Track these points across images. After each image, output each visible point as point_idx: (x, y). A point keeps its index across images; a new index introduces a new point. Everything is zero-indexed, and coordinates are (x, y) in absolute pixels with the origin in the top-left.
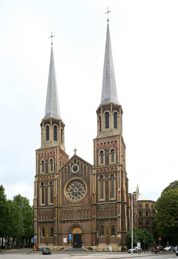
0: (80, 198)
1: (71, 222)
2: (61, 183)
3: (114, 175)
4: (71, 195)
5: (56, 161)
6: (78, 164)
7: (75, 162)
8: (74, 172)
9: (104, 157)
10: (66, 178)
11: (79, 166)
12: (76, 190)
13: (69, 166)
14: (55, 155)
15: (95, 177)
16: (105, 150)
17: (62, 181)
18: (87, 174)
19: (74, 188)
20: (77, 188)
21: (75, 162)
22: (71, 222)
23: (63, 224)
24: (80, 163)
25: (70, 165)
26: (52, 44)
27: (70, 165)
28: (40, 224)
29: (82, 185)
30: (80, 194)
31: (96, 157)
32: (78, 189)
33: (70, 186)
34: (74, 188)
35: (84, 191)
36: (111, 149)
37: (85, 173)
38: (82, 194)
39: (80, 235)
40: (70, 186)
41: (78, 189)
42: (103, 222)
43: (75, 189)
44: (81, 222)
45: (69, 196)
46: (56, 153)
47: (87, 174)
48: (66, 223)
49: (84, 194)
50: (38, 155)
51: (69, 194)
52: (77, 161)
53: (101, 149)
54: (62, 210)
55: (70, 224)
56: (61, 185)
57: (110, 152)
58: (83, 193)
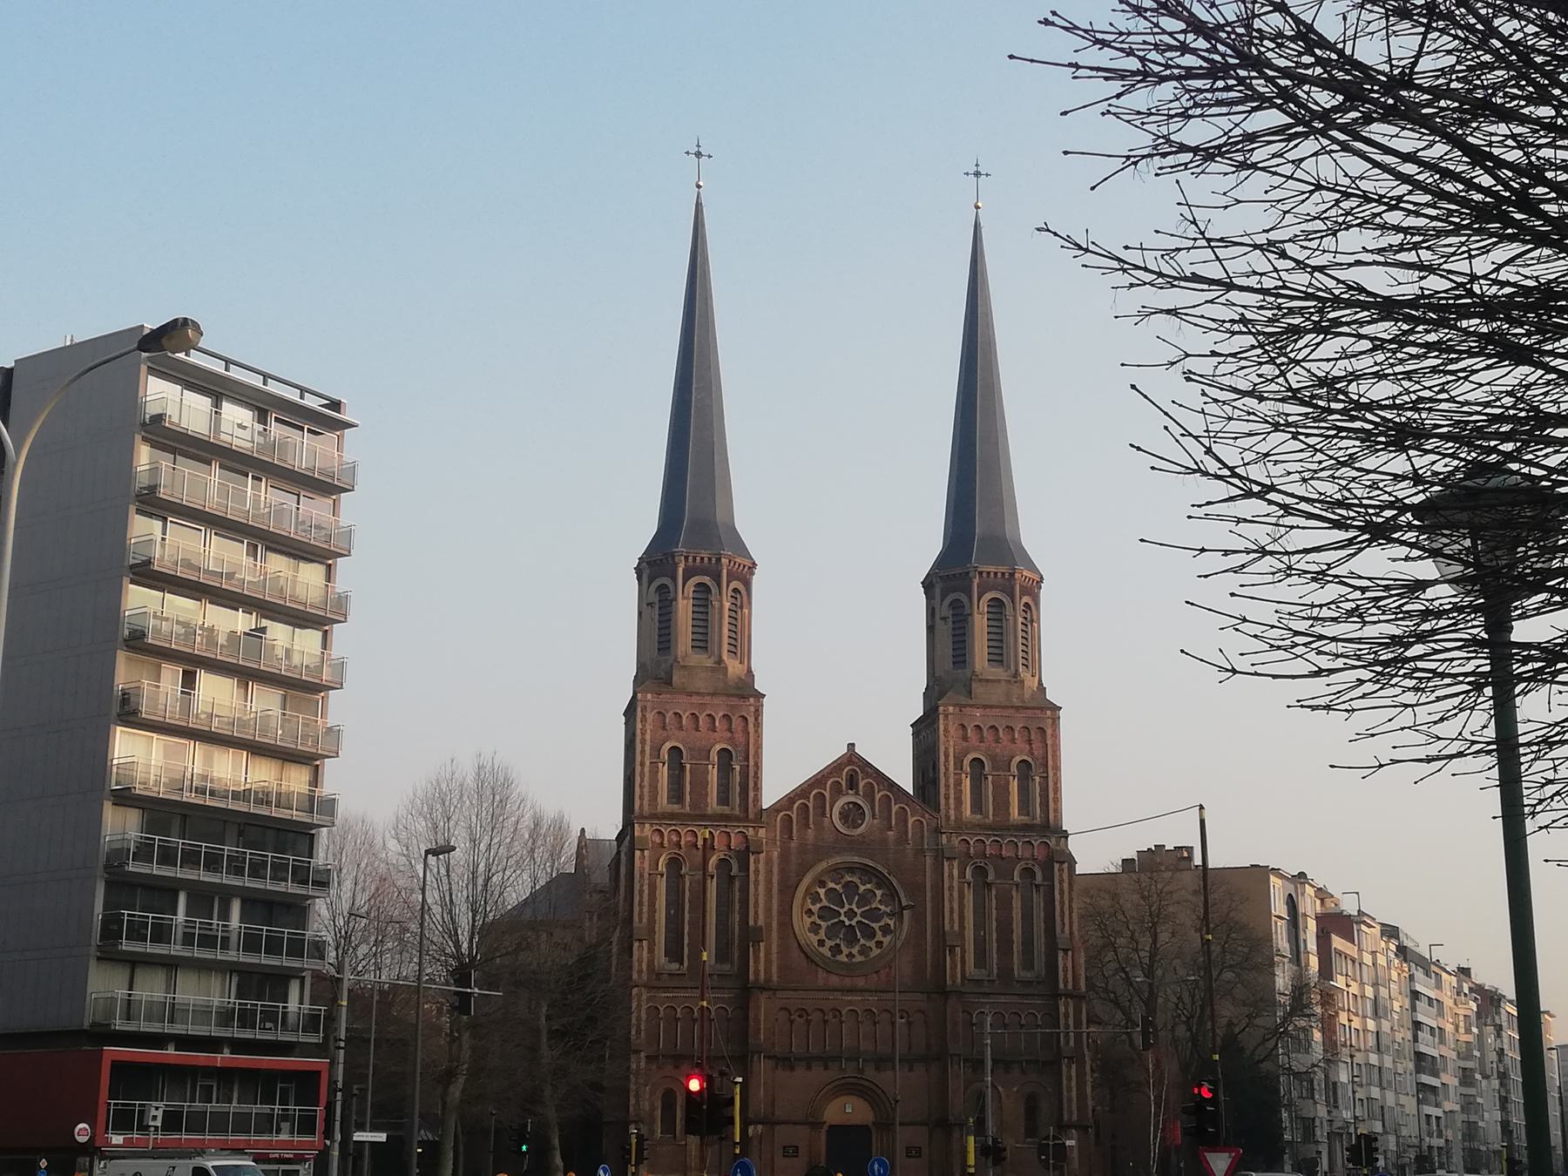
0: (811, 935)
1: (826, 1068)
3: (1033, 874)
4: (822, 932)
7: (852, 783)
8: (838, 825)
11: (873, 809)
12: (851, 914)
16: (993, 758)
19: (863, 915)
20: (858, 918)
21: (852, 783)
22: (826, 1068)
27: (827, 795)
28: (654, 1067)
29: (879, 893)
30: (871, 934)
31: (952, 781)
34: (863, 915)
35: (892, 923)
38: (879, 933)
39: (863, 1130)
40: (822, 891)
41: (859, 911)
43: (847, 907)
45: (814, 939)
49: (889, 938)
51: (815, 928)
53: (976, 749)
57: (1014, 769)
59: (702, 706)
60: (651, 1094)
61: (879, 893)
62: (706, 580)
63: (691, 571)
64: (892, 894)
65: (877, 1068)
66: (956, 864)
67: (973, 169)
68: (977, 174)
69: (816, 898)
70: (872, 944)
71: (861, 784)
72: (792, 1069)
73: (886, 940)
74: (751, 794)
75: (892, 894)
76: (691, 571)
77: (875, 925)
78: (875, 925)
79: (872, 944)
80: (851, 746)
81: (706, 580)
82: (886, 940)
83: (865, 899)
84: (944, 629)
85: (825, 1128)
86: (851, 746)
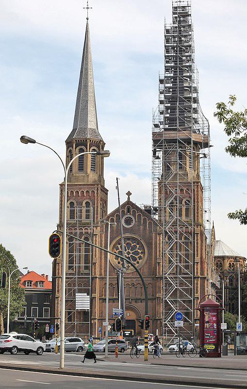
5: (96, 206)
6: (134, 215)
7: (129, 211)
15: (161, 239)
19: (133, 253)
20: (131, 254)
21: (129, 211)
22: (114, 302)
24: (137, 215)
26: (87, 19)
29: (138, 246)
32: (131, 252)
33: (140, 251)
35: (142, 256)
41: (131, 252)
44: (136, 302)
58: (140, 258)
61: (138, 246)
63: (85, 148)
64: (142, 247)
67: (86, 7)
68: (88, 8)
69: (117, 249)
70: (136, 263)
71: (131, 211)
73: (140, 261)
75: (142, 247)
76: (85, 148)
77: (137, 257)
78: (137, 257)
79: (136, 263)
82: (140, 261)
83: (133, 248)
84: (31, 140)
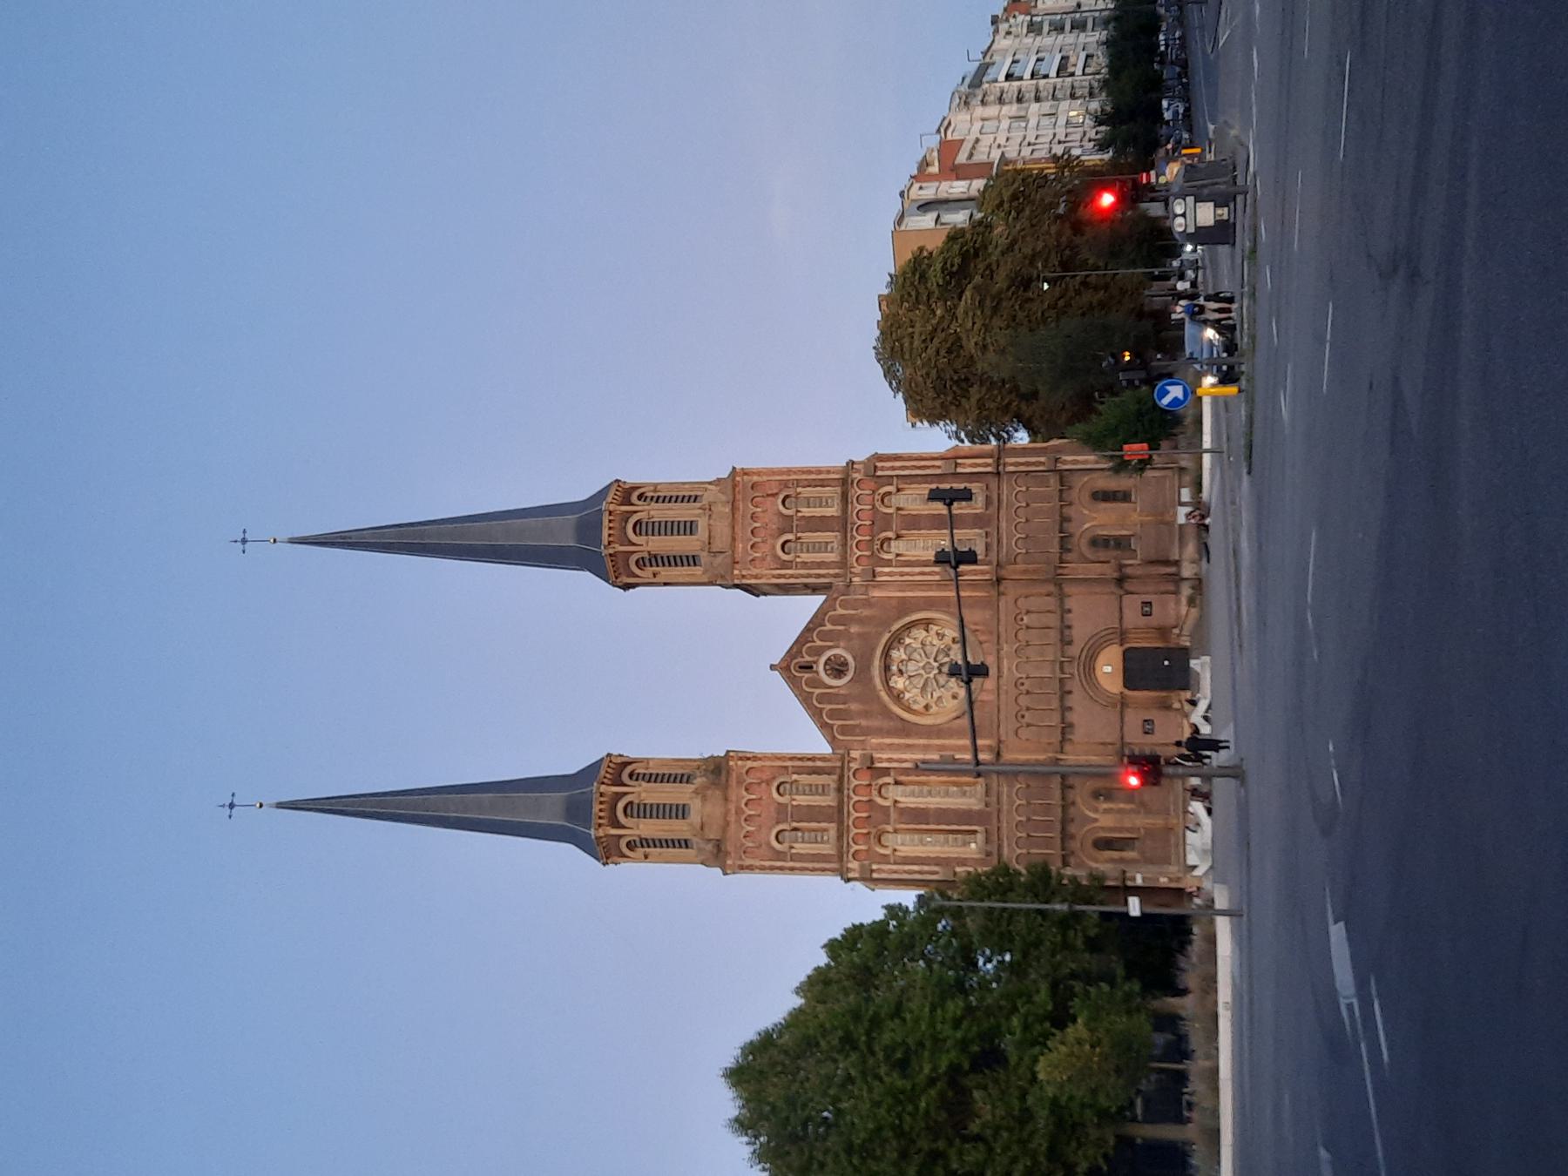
2: (888, 741)
5: (789, 763)
6: (819, 652)
7: (807, 667)
9: (808, 537)
10: (866, 714)
11: (830, 648)
13: (821, 698)
14: (761, 769)
15: (887, 570)
16: (782, 532)
17: (880, 732)
18: (866, 612)
21: (807, 667)
23: (1078, 735)
24: (819, 643)
25: (818, 691)
36: (781, 507)
37: (860, 621)
42: (1075, 539)
46: (755, 764)
47: (866, 612)
48: (1072, 717)
50: (748, 862)
52: (808, 658)
54: (1011, 733)
55: (1076, 699)
56: (896, 741)
59: (739, 811)
60: (1096, 861)
62: (621, 805)
65: (1070, 643)
66: (879, 569)
68: (232, 806)
72: (1071, 725)
74: (819, 764)
80: (772, 667)
81: (621, 805)
85: (1127, 692)
86: (772, 667)
